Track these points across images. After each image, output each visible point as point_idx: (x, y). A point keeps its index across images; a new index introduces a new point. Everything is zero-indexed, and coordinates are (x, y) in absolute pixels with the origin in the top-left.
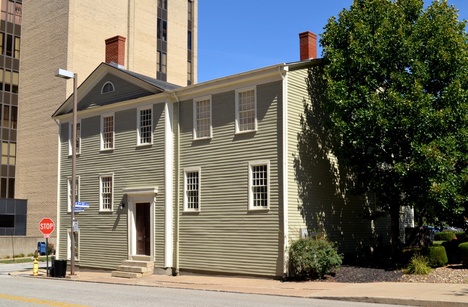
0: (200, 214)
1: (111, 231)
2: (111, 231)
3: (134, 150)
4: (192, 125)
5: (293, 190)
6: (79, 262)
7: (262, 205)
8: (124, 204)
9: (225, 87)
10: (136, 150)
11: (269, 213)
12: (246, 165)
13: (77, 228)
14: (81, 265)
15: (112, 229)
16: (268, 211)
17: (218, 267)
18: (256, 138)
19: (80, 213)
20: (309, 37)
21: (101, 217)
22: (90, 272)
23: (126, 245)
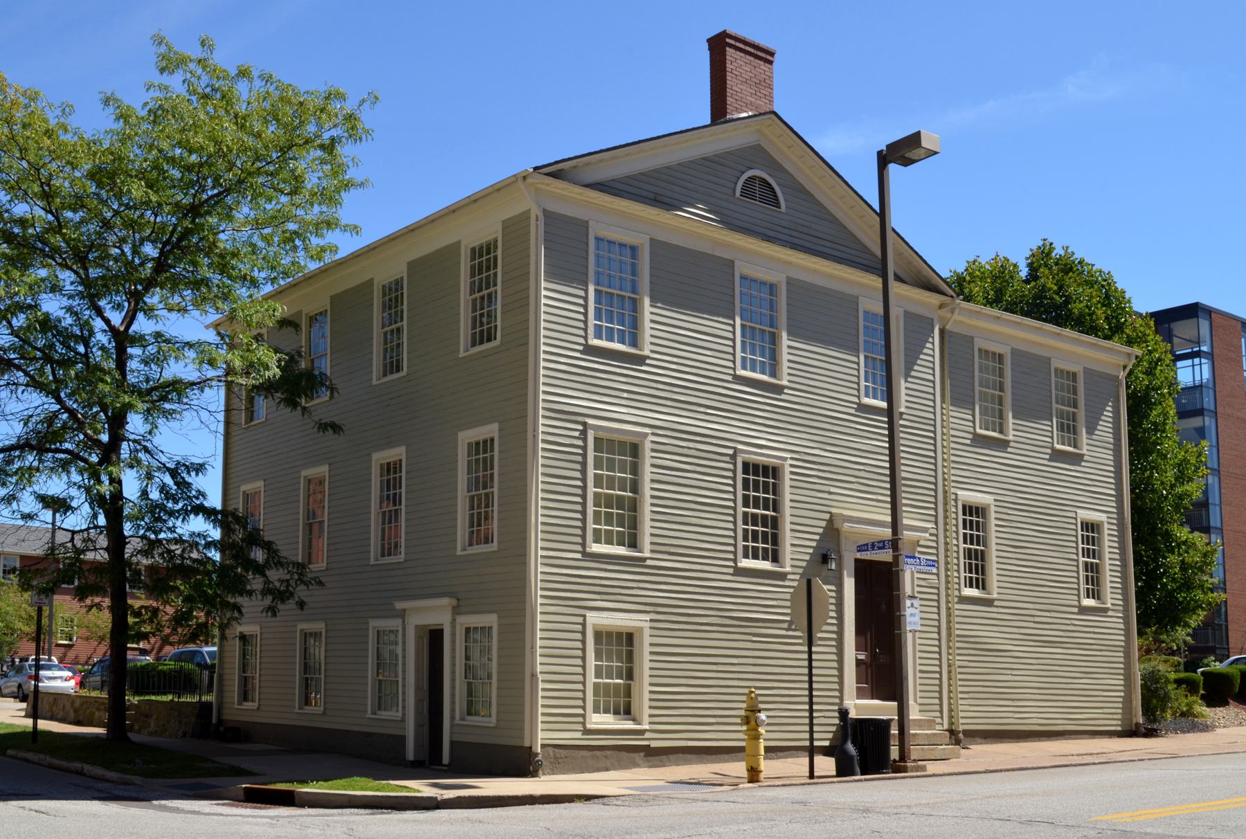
0: (996, 603)
1: (784, 632)
2: (784, 632)
3: (853, 411)
4: (734, 310)
5: (726, 533)
6: (647, 735)
7: (978, 587)
8: (824, 558)
9: (1041, 345)
10: (857, 410)
11: (1110, 613)
12: (1073, 515)
13: (917, 619)
14: (654, 744)
15: (785, 625)
16: (1106, 610)
17: (1033, 721)
18: (1084, 467)
19: (649, 562)
20: (729, 51)
21: (742, 584)
22: (697, 763)
23: (580, 687)
